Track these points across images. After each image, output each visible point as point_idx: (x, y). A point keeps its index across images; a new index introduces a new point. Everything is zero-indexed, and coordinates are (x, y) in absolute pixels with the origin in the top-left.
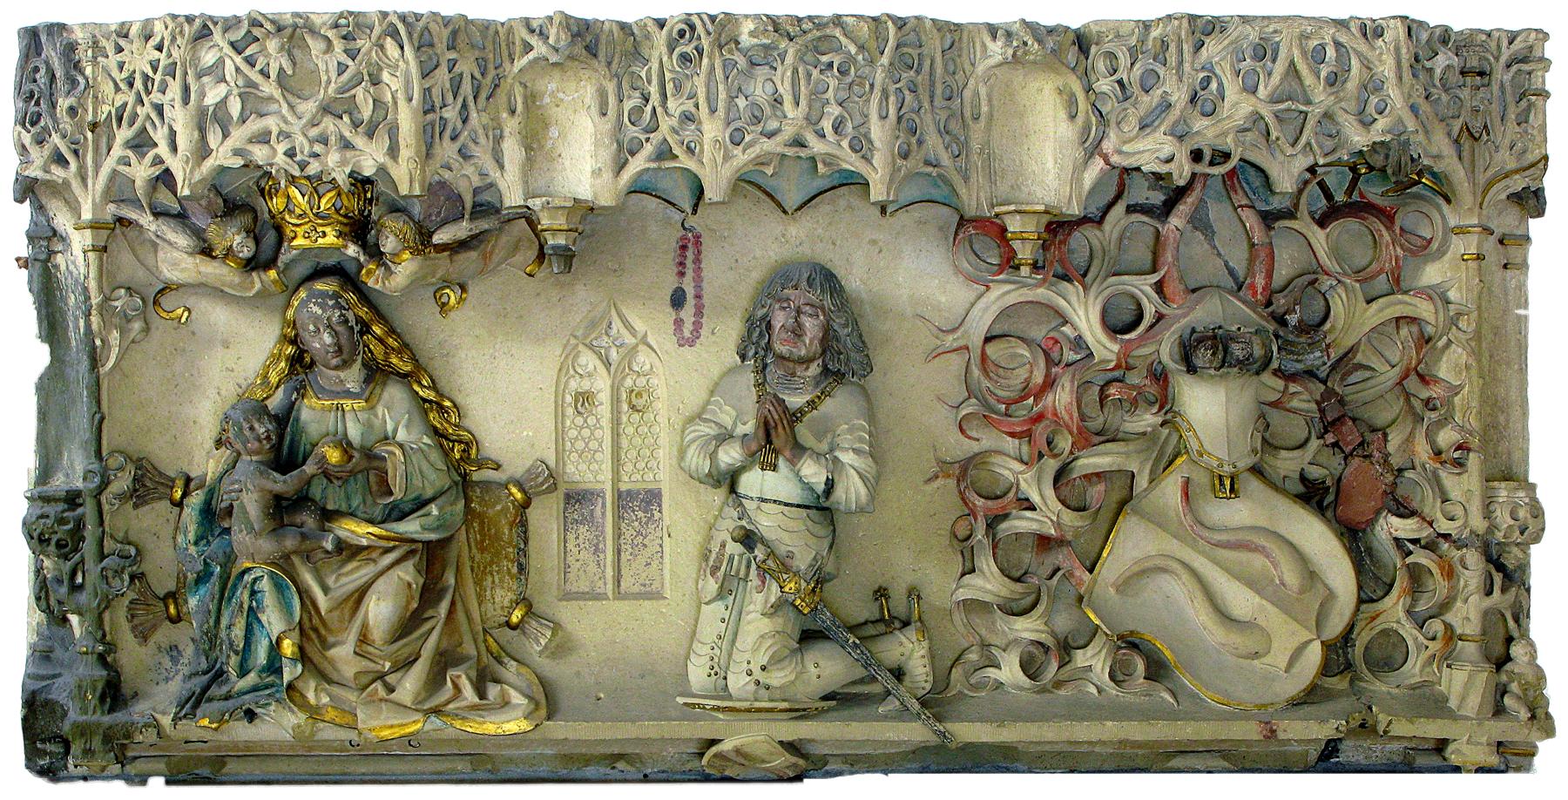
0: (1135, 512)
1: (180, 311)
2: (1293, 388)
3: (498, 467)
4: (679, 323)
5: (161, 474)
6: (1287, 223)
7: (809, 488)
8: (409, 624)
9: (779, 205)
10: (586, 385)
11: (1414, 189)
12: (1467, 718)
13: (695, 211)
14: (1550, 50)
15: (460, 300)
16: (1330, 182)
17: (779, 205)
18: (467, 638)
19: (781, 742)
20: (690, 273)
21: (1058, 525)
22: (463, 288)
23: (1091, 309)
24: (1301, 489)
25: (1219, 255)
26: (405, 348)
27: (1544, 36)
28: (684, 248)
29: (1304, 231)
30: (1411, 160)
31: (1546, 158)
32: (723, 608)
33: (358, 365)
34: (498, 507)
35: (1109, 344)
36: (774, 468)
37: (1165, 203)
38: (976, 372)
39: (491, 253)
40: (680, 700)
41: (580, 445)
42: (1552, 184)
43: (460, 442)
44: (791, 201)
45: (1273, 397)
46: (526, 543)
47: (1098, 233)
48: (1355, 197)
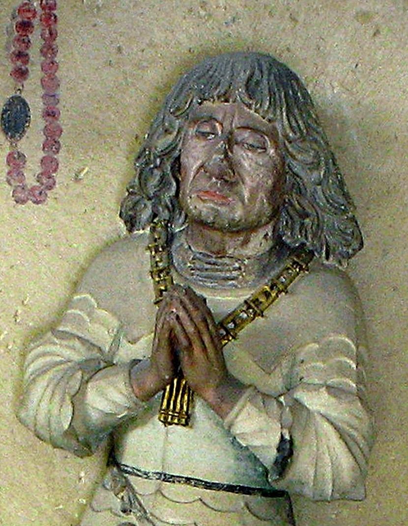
7: (249, 455)
20: (35, 72)
28: (25, 26)
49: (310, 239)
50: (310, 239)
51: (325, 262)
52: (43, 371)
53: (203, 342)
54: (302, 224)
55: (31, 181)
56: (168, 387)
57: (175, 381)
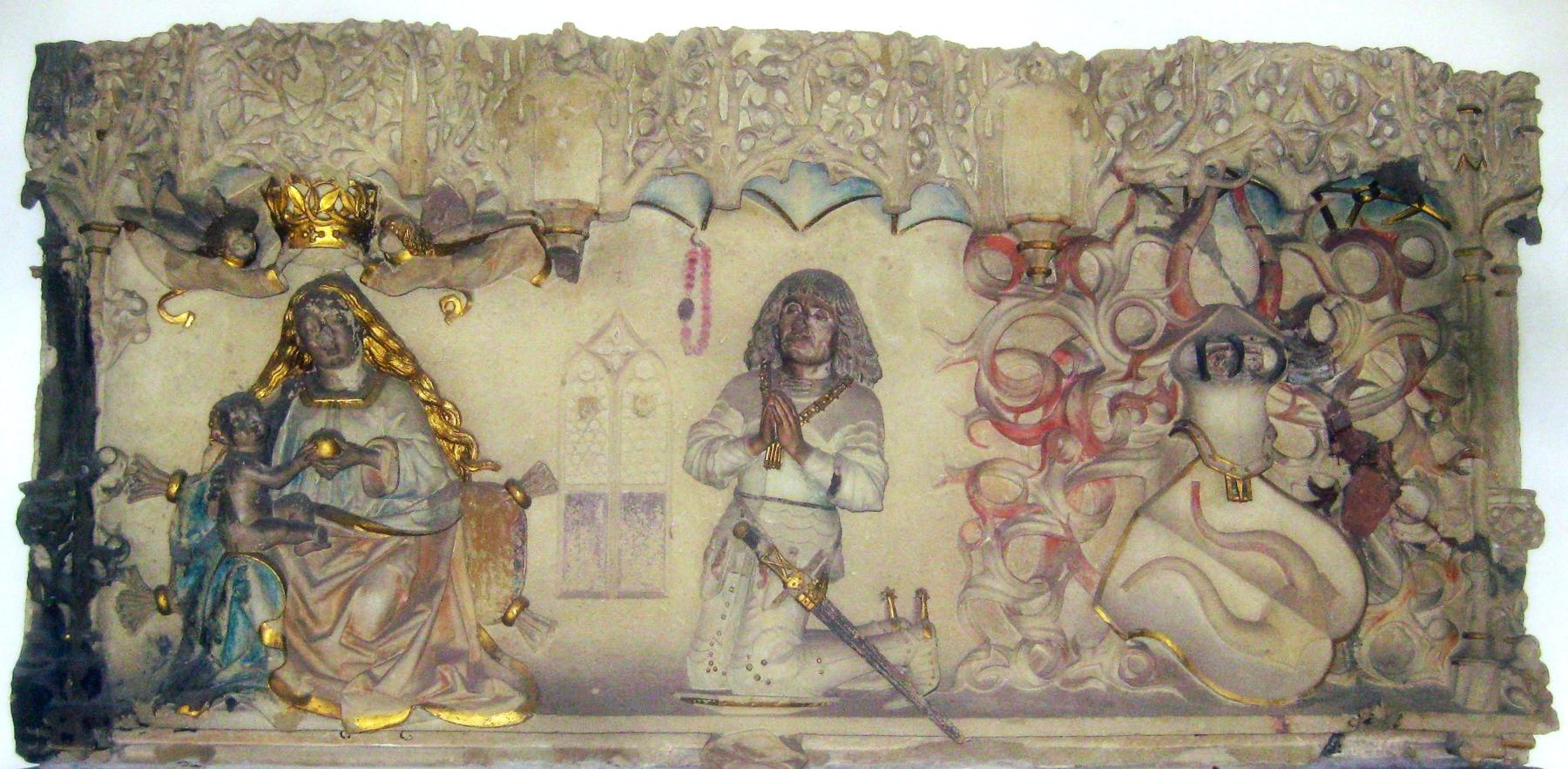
0: (1152, 517)
1: (184, 316)
2: (1301, 401)
3: (496, 468)
4: (686, 333)
5: (157, 470)
6: (1294, 245)
7: (818, 484)
8: (394, 619)
9: (789, 221)
10: (590, 391)
11: (1413, 218)
12: (1474, 712)
13: (704, 225)
14: (1540, 92)
15: (466, 309)
16: (1334, 209)
17: (789, 221)
18: (459, 632)
19: (781, 738)
20: (698, 284)
21: (1068, 529)
22: (469, 296)
23: (1101, 322)
24: (1311, 497)
25: (1226, 276)
26: (403, 352)
27: (1533, 80)
28: (692, 261)
29: (1309, 253)
30: (1389, 203)
31: (1540, 188)
32: (722, 603)
33: (355, 367)
34: (496, 506)
35: (1120, 355)
36: (778, 466)
37: (1173, 226)
38: (985, 382)
39: (497, 262)
40: (678, 696)
41: (582, 448)
42: (1547, 213)
43: (460, 443)
44: (802, 217)
45: (1282, 409)
46: (524, 541)
47: (1108, 252)
48: (1357, 225)
52: (1284, 566)
55: (694, 341)
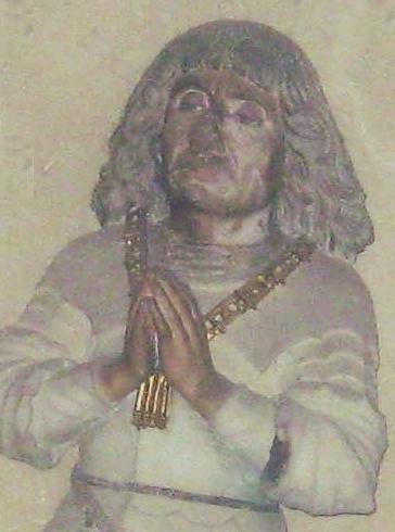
7: (243, 459)
49: (312, 230)
50: (312, 230)
51: (330, 255)
53: (183, 330)
54: (303, 214)
56: (143, 386)
57: (152, 379)
